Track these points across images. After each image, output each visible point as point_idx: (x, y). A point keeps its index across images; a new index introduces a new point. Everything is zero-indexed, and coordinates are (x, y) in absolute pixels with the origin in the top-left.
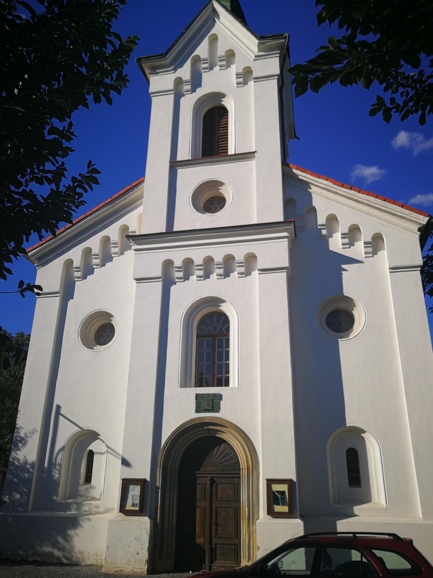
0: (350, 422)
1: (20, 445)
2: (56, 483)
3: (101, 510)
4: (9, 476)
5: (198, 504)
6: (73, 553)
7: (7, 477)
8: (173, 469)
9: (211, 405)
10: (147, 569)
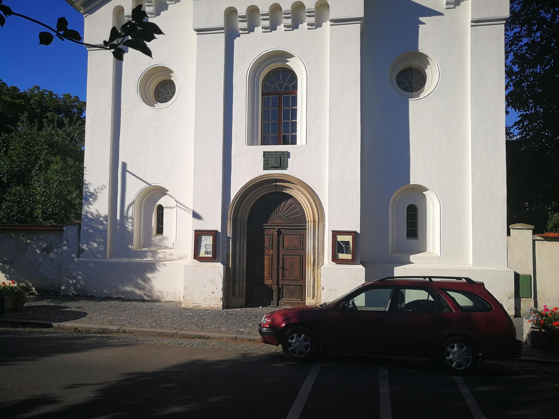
0: (414, 180)
1: (91, 199)
2: (131, 234)
3: (175, 257)
4: (84, 228)
6: (152, 292)
7: (82, 228)
10: (223, 305)
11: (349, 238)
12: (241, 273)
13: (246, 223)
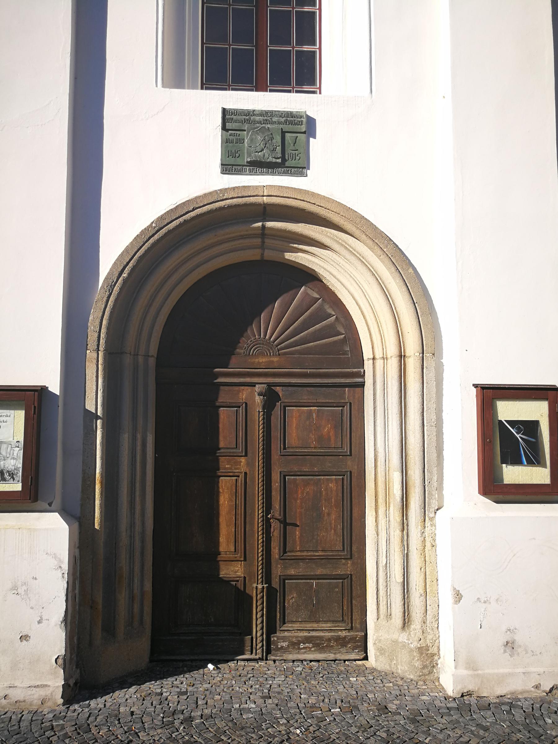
5: (225, 464)
8: (141, 359)
9: (279, 149)
11: (537, 411)
12: (138, 544)
13: (152, 362)
